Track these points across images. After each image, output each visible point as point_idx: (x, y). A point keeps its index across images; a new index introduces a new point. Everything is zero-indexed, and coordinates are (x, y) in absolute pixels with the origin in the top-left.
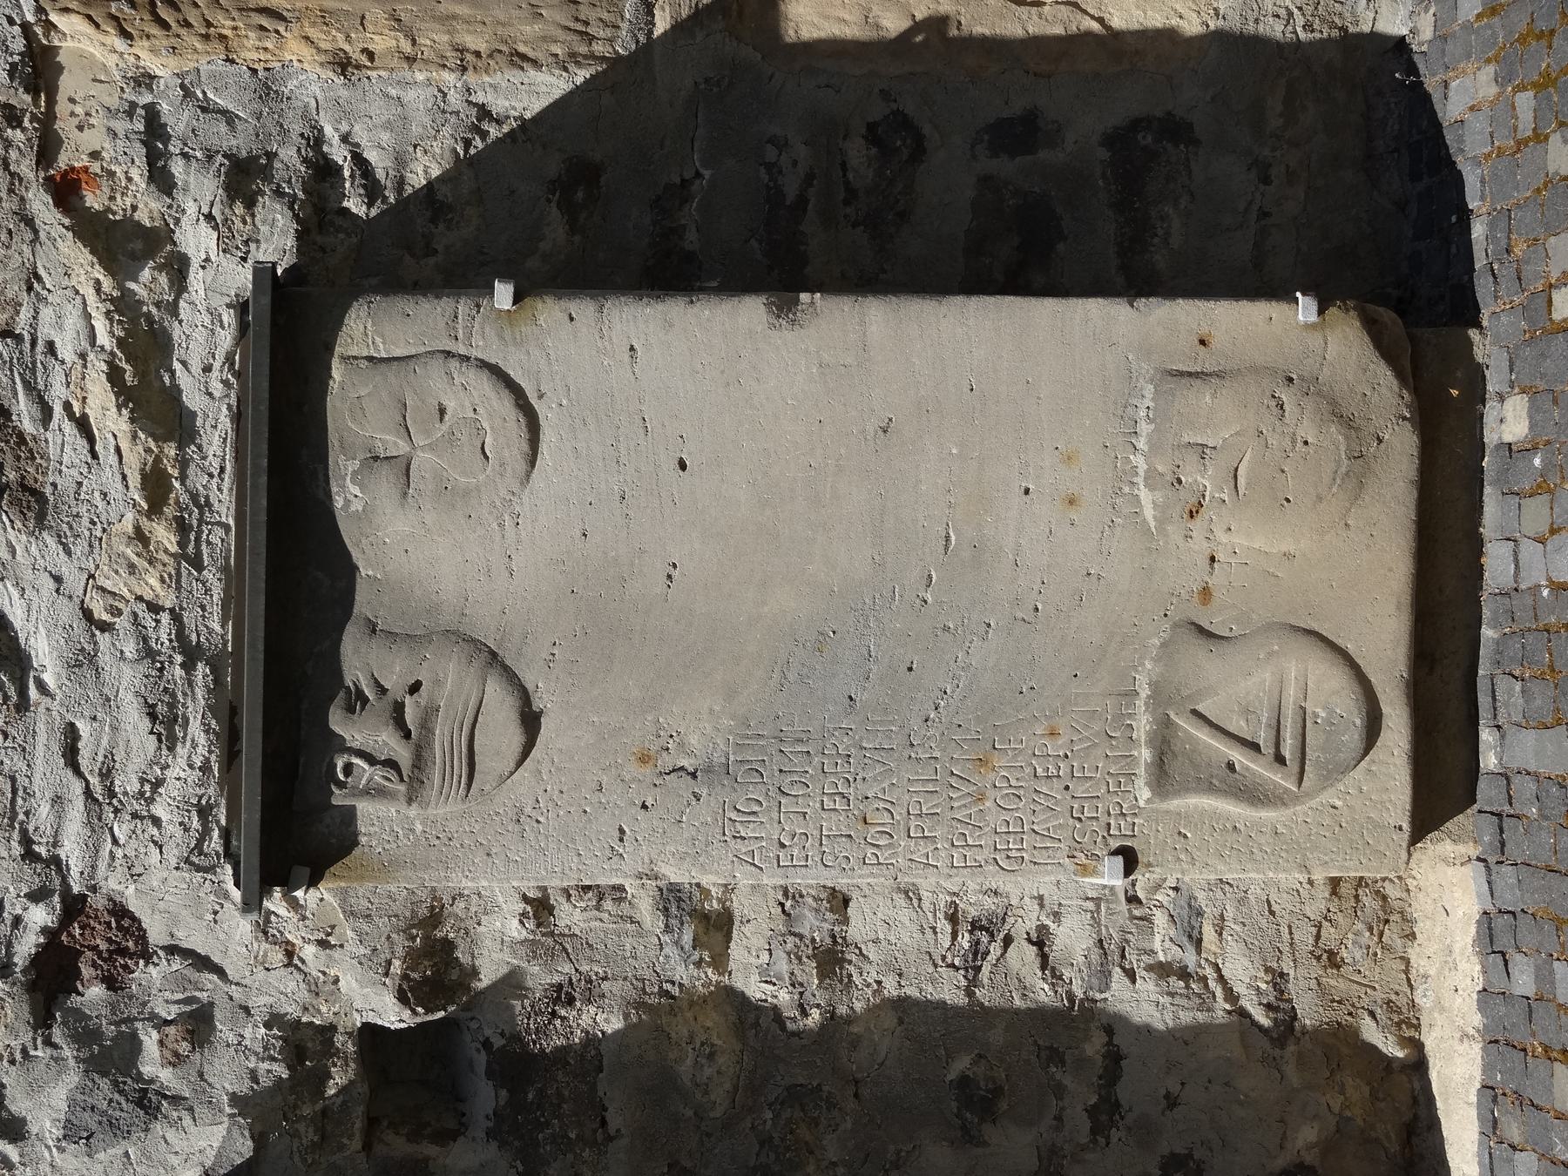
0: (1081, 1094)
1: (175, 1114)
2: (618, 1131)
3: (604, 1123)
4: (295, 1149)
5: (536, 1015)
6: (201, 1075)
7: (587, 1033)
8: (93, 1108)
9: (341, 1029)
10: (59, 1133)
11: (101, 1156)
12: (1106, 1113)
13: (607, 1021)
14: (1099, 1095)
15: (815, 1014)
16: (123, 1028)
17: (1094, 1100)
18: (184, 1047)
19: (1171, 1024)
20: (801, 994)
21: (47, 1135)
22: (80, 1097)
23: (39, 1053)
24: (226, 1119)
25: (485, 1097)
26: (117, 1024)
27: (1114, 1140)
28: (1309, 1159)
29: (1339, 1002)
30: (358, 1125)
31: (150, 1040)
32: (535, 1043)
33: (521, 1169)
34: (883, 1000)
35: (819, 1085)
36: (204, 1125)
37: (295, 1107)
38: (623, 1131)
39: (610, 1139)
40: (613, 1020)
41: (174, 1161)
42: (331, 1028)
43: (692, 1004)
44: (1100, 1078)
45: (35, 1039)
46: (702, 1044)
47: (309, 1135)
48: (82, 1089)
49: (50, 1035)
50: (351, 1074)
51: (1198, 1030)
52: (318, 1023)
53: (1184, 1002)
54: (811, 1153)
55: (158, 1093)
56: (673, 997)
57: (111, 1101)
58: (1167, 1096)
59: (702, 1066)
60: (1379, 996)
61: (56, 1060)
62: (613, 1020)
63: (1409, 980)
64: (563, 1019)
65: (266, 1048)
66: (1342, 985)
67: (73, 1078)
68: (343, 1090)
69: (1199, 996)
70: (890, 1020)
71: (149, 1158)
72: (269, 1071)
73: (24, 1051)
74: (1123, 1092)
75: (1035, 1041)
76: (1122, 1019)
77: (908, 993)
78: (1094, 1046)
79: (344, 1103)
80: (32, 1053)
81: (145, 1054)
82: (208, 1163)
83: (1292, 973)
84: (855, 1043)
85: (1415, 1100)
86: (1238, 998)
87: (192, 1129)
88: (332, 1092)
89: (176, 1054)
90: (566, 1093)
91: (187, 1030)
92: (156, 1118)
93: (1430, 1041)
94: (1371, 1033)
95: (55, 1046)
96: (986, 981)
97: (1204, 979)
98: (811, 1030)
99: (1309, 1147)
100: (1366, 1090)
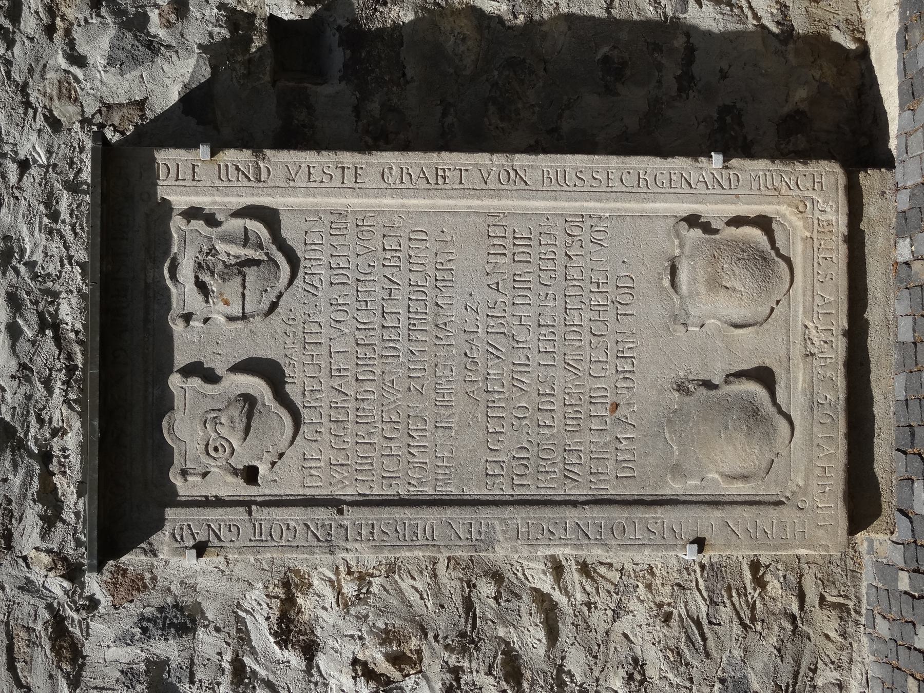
0: (672, 70)
1: (168, 54)
2: (412, 78)
3: (404, 75)
4: (234, 76)
5: (366, 9)
6: (182, 35)
7: (394, 22)
8: (123, 49)
9: (258, 17)
10: (104, 62)
11: (128, 76)
12: (686, 81)
13: (405, 15)
14: (683, 70)
15: (521, 18)
16: (140, 9)
17: (679, 72)
18: (173, 18)
19: (722, 30)
20: (514, 6)
21: (99, 65)
22: (116, 42)
23: (94, 21)
24: (196, 55)
25: (338, 57)
26: (136, 8)
27: (691, 97)
28: (802, 107)
29: (819, 21)
30: (268, 68)
31: (154, 15)
32: (365, 25)
33: (358, 95)
34: (559, 14)
35: (524, 59)
36: (184, 59)
37: (233, 56)
38: (415, 78)
39: (408, 82)
40: (409, 14)
41: (167, 81)
42: (252, 16)
43: (452, 13)
44: (683, 60)
45: (91, 14)
46: (459, 33)
47: (242, 71)
48: (117, 37)
49: (100, 12)
50: (264, 41)
51: (737, 35)
52: (246, 11)
53: (730, 18)
54: (521, 99)
55: (158, 43)
56: (442, 7)
57: (133, 45)
58: (721, 71)
59: (459, 45)
60: (841, 18)
61: (103, 24)
62: (409, 14)
63: (858, 7)
64: (381, 12)
65: (217, 21)
66: (820, 12)
67: (112, 31)
68: (259, 49)
69: (739, 16)
70: (563, 27)
71: (154, 79)
72: (219, 33)
73: (86, 20)
74: (696, 69)
75: (646, 40)
76: (695, 28)
77: (574, 11)
78: (679, 42)
79: (260, 56)
80: (90, 21)
81: (151, 22)
82: (186, 81)
83: (791, 5)
84: (544, 36)
85: (863, 75)
86: (760, 18)
87: (177, 62)
88: (254, 50)
89: (168, 21)
90: (383, 56)
91: (174, 8)
92: (158, 55)
93: (870, 38)
94: (837, 36)
95: (103, 17)
96: (617, 5)
97: (741, 7)
98: (519, 26)
99: (802, 100)
100: (835, 70)
